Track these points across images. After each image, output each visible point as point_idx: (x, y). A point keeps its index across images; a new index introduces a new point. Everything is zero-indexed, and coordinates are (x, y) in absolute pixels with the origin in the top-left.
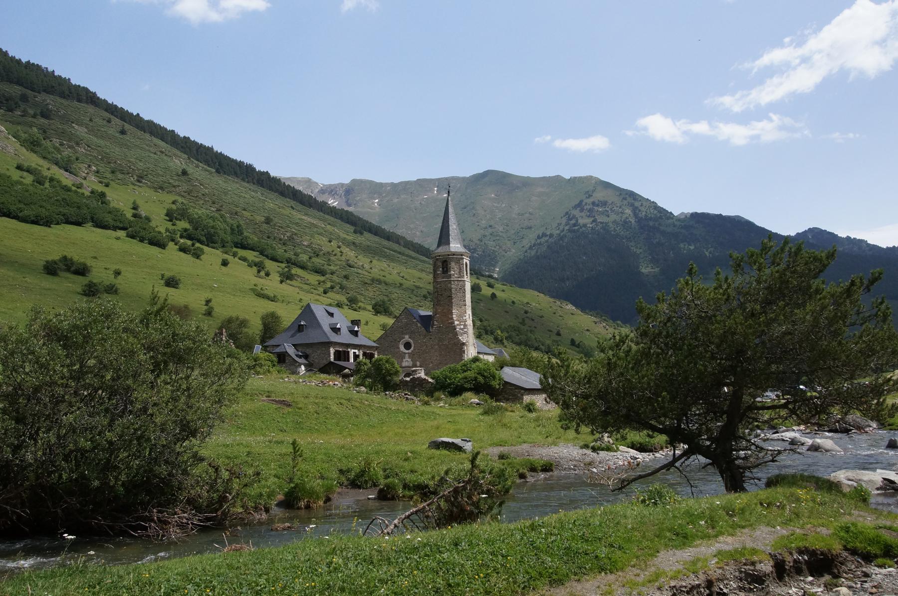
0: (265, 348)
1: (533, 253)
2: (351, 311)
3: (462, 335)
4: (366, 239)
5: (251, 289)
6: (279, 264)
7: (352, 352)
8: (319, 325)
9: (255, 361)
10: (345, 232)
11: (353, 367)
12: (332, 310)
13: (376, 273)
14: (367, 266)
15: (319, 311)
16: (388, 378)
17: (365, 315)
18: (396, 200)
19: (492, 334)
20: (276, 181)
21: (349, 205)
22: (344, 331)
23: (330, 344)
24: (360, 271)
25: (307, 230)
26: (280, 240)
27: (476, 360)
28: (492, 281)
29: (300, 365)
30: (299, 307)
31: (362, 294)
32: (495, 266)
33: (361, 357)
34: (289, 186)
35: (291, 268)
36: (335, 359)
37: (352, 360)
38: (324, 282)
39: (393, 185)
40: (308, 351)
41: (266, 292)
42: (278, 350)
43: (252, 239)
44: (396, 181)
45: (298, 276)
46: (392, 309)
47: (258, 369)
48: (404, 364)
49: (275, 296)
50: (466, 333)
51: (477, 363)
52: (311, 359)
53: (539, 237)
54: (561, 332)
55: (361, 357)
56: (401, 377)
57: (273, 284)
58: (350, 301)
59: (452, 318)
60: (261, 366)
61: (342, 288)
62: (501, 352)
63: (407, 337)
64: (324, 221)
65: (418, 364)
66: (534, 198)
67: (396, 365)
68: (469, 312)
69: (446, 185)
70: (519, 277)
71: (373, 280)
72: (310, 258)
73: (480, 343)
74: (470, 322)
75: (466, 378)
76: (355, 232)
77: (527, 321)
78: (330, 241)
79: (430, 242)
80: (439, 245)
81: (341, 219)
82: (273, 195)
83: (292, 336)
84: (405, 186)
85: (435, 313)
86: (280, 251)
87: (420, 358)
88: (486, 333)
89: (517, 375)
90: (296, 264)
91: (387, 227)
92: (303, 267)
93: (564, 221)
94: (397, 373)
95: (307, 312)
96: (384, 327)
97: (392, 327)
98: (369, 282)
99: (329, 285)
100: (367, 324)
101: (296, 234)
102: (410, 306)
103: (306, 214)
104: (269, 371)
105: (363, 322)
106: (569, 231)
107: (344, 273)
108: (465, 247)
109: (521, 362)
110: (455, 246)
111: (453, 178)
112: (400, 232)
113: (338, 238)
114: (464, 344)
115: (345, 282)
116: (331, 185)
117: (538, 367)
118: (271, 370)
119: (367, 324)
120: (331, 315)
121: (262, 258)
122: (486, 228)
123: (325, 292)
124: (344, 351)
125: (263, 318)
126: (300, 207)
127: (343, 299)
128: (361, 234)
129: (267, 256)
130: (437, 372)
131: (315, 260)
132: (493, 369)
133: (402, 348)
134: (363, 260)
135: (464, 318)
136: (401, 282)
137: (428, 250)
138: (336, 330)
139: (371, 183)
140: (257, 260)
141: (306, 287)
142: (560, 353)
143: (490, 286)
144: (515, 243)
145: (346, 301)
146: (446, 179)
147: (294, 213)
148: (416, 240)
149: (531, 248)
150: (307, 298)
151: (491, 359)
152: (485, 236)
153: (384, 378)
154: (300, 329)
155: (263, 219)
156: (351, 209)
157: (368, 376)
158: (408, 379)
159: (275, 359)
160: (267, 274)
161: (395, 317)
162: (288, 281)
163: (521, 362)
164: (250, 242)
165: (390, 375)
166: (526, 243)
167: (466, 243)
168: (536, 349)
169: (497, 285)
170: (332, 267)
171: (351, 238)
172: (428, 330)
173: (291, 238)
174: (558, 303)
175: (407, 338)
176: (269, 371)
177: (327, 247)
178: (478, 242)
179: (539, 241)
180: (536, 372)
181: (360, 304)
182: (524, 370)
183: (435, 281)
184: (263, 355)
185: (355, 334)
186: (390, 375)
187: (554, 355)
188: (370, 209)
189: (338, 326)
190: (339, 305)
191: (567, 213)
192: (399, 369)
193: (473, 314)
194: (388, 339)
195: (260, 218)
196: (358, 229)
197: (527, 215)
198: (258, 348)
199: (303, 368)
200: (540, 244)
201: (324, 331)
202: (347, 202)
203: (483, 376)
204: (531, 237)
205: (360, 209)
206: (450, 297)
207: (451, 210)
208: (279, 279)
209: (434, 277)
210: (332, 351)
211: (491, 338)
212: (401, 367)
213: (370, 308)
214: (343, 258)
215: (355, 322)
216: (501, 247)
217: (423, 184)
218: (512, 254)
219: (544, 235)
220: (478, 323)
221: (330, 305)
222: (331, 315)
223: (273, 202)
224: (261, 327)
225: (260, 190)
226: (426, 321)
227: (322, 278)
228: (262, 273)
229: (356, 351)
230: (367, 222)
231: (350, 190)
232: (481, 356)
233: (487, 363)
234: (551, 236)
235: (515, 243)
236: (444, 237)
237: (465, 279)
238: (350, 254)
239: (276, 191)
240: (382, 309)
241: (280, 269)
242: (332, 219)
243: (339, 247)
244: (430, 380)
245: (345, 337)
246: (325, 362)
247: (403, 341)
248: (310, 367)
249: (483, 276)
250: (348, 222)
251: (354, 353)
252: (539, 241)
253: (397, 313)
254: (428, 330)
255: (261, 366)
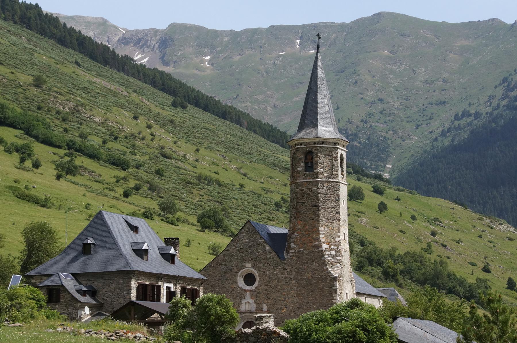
0: (28, 280)
1: (447, 142)
2: (165, 224)
3: (332, 264)
4: (194, 115)
5: (10, 188)
6: (56, 150)
7: (164, 286)
8: (115, 245)
9: (11, 300)
10: (157, 103)
11: (165, 310)
12: (135, 221)
13: (204, 168)
14: (191, 157)
15: (116, 223)
16: (219, 328)
17: (186, 231)
18: (237, 58)
19: (379, 265)
20: (52, 21)
21: (166, 64)
22: (154, 254)
23: (131, 274)
24: (180, 164)
25: (101, 100)
26: (58, 112)
27: (354, 304)
28: (380, 184)
29: (82, 307)
30: (85, 216)
31: (182, 199)
32: (385, 161)
33: (178, 294)
34: (72, 29)
35: (75, 154)
36: (138, 298)
37: (163, 299)
38: (124, 179)
39: (233, 34)
40: (97, 285)
41: (33, 192)
42: (49, 282)
43: (13, 110)
44: (238, 28)
45: (85, 169)
46: (227, 222)
47: (15, 313)
48: (244, 307)
49: (46, 199)
50: (339, 262)
51: (356, 311)
52: (100, 296)
53: (457, 118)
54: (491, 267)
55: (178, 294)
56: (239, 327)
57: (43, 180)
58: (163, 209)
59: (318, 239)
60: (19, 307)
61: (152, 188)
62: (393, 294)
63: (249, 265)
64: (127, 86)
65: (265, 307)
66: (451, 56)
67: (233, 310)
68: (344, 230)
69: (316, 36)
70: (422, 179)
71: (200, 178)
72: (104, 142)
73: (361, 280)
74: (345, 246)
75: (339, 332)
76: (174, 105)
77: (435, 247)
78: (136, 118)
79: (288, 123)
80: (301, 127)
81: (154, 84)
82: (47, 43)
83: (73, 260)
84: (250, 38)
85: (293, 231)
86: (57, 130)
87: (266, 297)
88: (371, 265)
89: (419, 332)
90: (80, 150)
91: (223, 98)
92: (93, 156)
93: (500, 92)
94: (232, 321)
95: (98, 224)
96: (214, 249)
97: (226, 250)
98: (193, 181)
99: (132, 183)
100: (188, 244)
101: (82, 105)
102: (254, 219)
103: (99, 75)
104: (32, 316)
105: (183, 241)
106: (508, 107)
107: (156, 167)
108: (340, 130)
109: (426, 311)
110: (326, 130)
111: (326, 25)
112: (241, 106)
113: (148, 113)
114: (335, 279)
115: (157, 181)
116: (138, 32)
117: (452, 320)
118: (36, 313)
119: (188, 244)
120: (135, 229)
121: (28, 140)
122: (373, 103)
123: (126, 195)
124: (153, 286)
125: (25, 232)
126: (89, 63)
127: (153, 205)
128: (184, 107)
129: (36, 138)
130: (292, 322)
131: (111, 145)
132: (381, 321)
133: (241, 283)
134: (184, 149)
135: (337, 239)
136: (242, 182)
137: (283, 135)
138: (141, 253)
139: (199, 29)
140: (20, 142)
141: (96, 186)
142: (490, 301)
143: (378, 191)
144: (418, 126)
145: (157, 208)
146: (315, 26)
147: (80, 71)
148: (267, 120)
149: (443, 134)
150: (97, 204)
151: (377, 304)
152: (371, 115)
153: (212, 328)
154: (86, 249)
155: (30, 79)
156: (168, 69)
157: (188, 325)
158: (249, 331)
159: (43, 296)
160: (36, 165)
161: (232, 234)
162: (69, 177)
163: (426, 311)
164: (9, 113)
165: (222, 323)
166: (436, 126)
167: (342, 125)
168: (450, 291)
169: (388, 191)
170: (137, 157)
171: (167, 113)
172: (281, 257)
173: (75, 111)
174: (486, 221)
175: (249, 267)
176: (32, 316)
177: (130, 126)
178: (361, 124)
179: (456, 123)
180: (451, 328)
181: (179, 214)
182: (430, 325)
183: (293, 183)
184: (25, 290)
185: (171, 259)
186: (222, 323)
187: (481, 303)
188: (198, 71)
189: (145, 247)
190: (147, 215)
191: (505, 80)
192: (236, 315)
193: (351, 234)
194: (220, 269)
195: (25, 78)
196: (179, 100)
197: (439, 83)
198: (16, 281)
199: (87, 310)
200: (459, 128)
201: (122, 255)
202: (162, 58)
203: (365, 329)
204: (443, 118)
205: (180, 70)
206: (316, 207)
207: (320, 74)
208: (55, 173)
209: (293, 177)
210: (134, 285)
211: (378, 271)
212: (239, 312)
213: (194, 219)
214: (155, 144)
215: (171, 242)
216: (395, 132)
217: (278, 34)
218: (413, 143)
219: (466, 114)
220: (358, 248)
221: (134, 214)
222: (135, 229)
223: (47, 54)
224: (23, 246)
225: (25, 32)
226: (279, 242)
227: (122, 174)
228: (28, 164)
229: (171, 285)
230: (193, 90)
231: (167, 40)
232: (362, 299)
233: (371, 310)
234: (477, 115)
235: (418, 126)
236: (309, 117)
237: (340, 179)
238: (165, 138)
239: (52, 37)
240: (213, 223)
241: (56, 158)
242: (140, 83)
243: (149, 127)
244: (283, 334)
245: (155, 264)
246: (122, 302)
247: (243, 272)
248: (97, 310)
249: (367, 176)
250: (163, 90)
251: (168, 288)
252: (456, 123)
253: (235, 229)
254: (281, 257)
255: (19, 307)
